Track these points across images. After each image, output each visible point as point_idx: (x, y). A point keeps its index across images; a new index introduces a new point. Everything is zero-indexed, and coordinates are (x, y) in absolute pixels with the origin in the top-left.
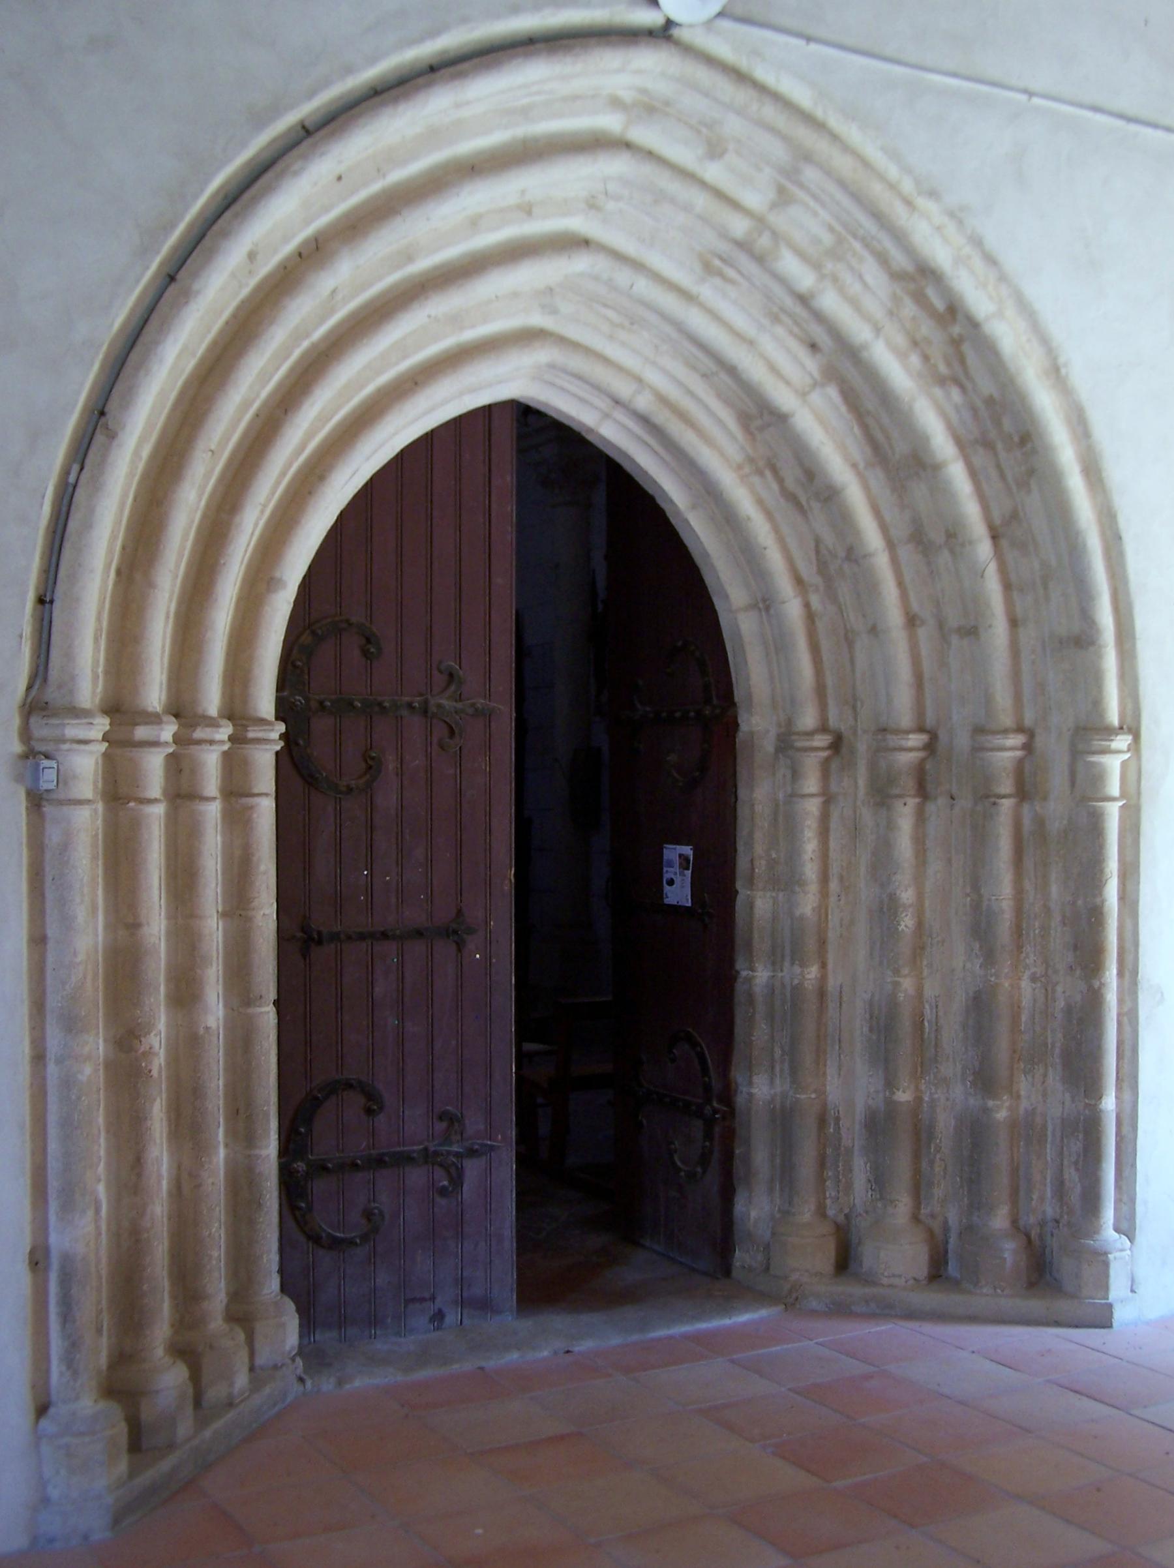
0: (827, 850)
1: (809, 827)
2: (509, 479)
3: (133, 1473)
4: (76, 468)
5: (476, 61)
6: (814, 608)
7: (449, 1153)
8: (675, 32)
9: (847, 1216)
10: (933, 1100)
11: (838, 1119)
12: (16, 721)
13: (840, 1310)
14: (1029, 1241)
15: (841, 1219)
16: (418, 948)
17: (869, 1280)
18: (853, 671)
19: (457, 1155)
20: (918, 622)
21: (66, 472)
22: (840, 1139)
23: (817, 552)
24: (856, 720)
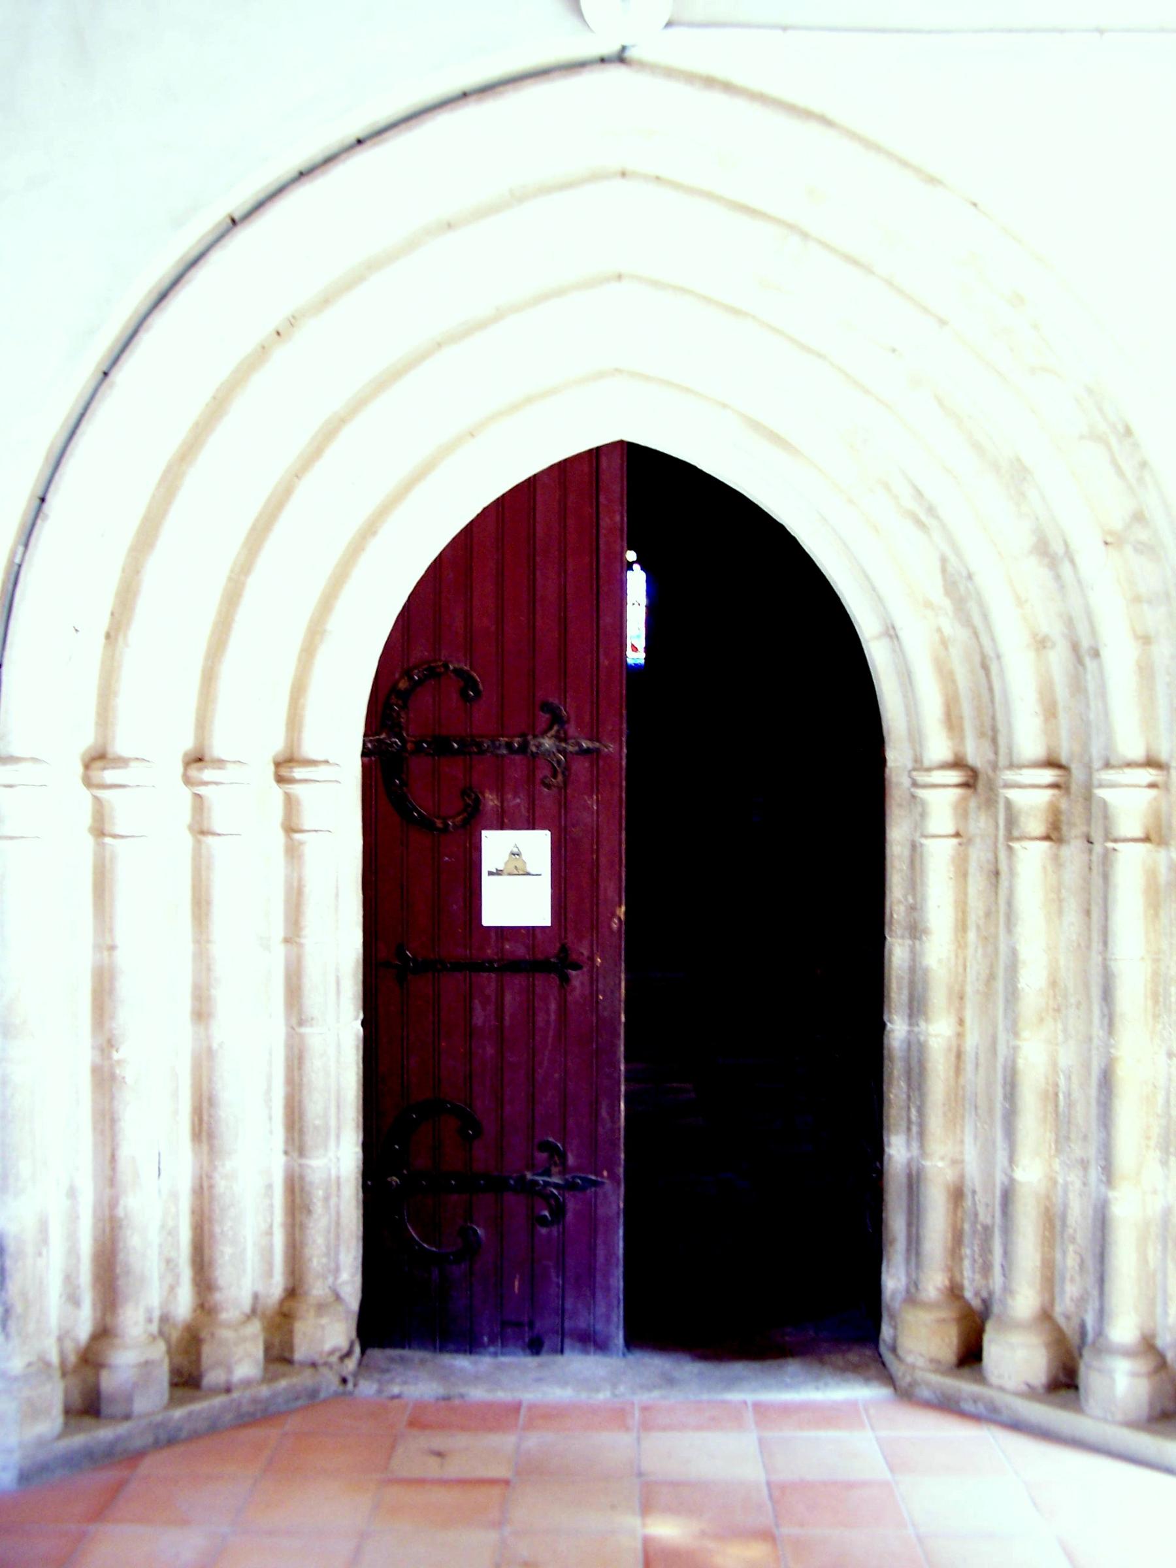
0: (966, 894)
1: (901, 870)
2: (618, 518)
3: (60, 1436)
4: (21, 549)
5: (403, 126)
6: (946, 634)
7: (547, 1184)
8: (628, 54)
9: (984, 1301)
10: (1066, 1184)
11: (974, 1192)
12: (80, 769)
13: (947, 1405)
14: (104, 1333)
15: (976, 1303)
16: (519, 980)
17: (981, 1379)
18: (992, 701)
19: (556, 1186)
20: (1049, 644)
21: (13, 553)
22: (976, 1215)
23: (944, 571)
24: (996, 753)
